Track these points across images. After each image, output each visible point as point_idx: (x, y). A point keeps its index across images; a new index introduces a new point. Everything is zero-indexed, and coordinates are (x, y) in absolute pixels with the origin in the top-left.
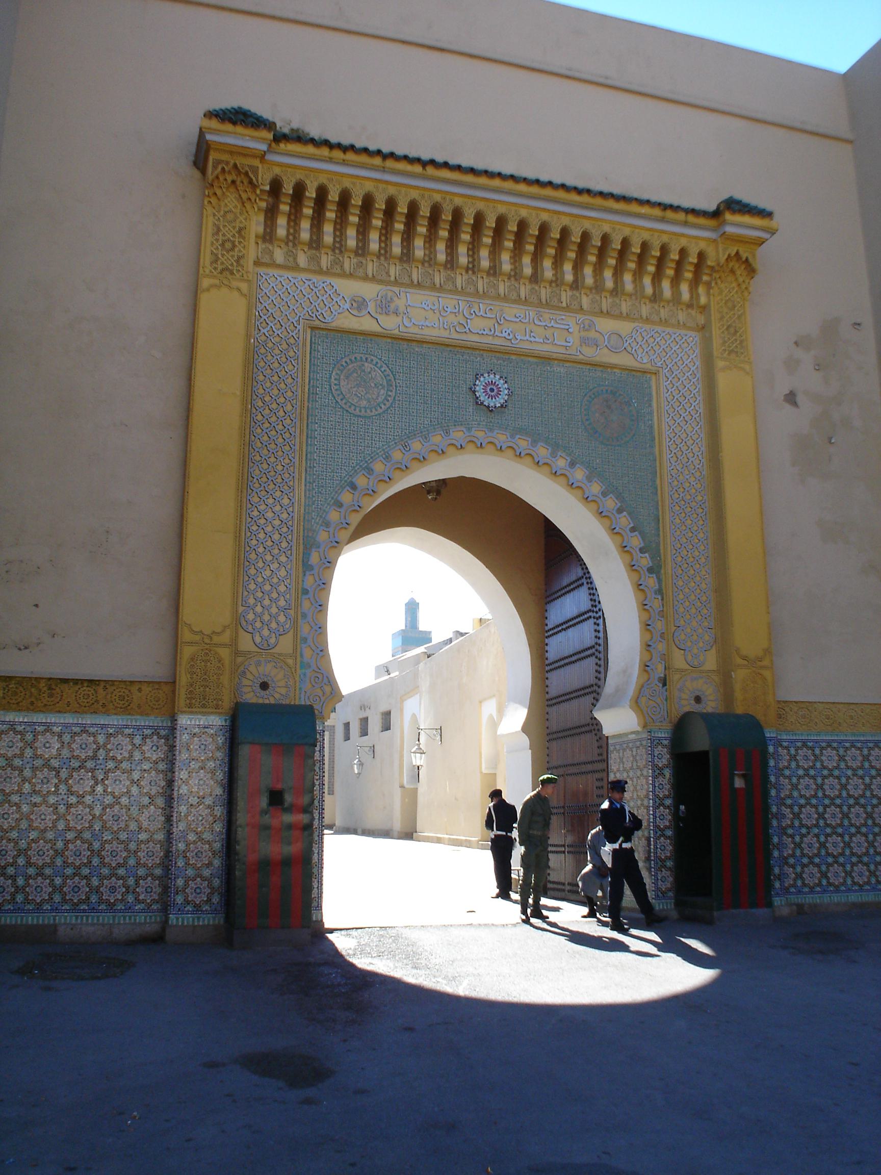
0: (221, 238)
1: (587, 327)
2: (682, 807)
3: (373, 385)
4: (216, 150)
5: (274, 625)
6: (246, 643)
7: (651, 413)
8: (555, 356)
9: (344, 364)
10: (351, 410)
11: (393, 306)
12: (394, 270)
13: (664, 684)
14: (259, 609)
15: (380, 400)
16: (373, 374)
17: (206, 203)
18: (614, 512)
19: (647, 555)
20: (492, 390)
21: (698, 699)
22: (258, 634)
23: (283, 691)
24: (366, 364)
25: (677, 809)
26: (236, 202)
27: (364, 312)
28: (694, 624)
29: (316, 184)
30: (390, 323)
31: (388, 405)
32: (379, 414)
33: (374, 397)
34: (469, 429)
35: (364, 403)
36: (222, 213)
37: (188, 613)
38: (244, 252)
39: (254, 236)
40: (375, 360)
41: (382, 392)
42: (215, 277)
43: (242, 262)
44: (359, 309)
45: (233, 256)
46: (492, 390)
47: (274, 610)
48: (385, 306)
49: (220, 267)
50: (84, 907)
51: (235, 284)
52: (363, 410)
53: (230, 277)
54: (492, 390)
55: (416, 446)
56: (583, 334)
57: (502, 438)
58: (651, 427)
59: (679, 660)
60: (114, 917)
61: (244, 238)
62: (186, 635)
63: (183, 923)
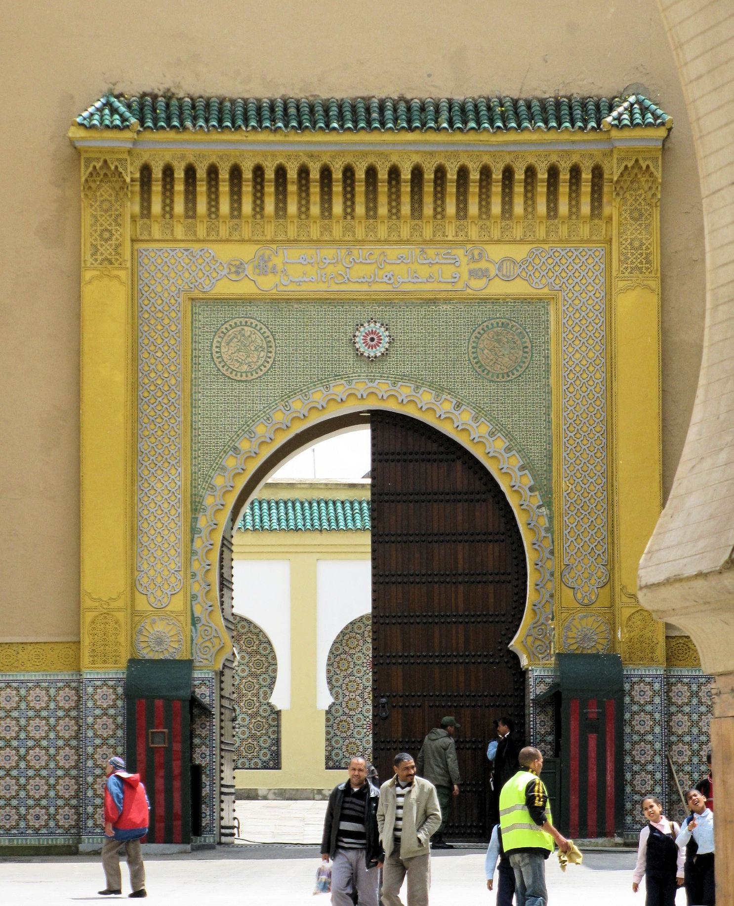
0: (99, 228)
1: (476, 257)
3: (253, 348)
4: (86, 152)
6: (142, 604)
9: (225, 331)
10: (233, 376)
11: (270, 265)
12: (270, 230)
15: (260, 362)
17: (82, 196)
18: (503, 452)
19: (537, 493)
20: (373, 339)
22: (152, 596)
24: (246, 328)
26: (110, 191)
27: (242, 275)
29: (183, 165)
30: (268, 284)
31: (268, 366)
32: (260, 377)
34: (350, 382)
35: (245, 368)
36: (98, 203)
37: (88, 584)
38: (116, 265)
39: (129, 216)
40: (255, 322)
41: (262, 354)
42: (95, 269)
43: (119, 250)
44: (237, 273)
45: (111, 245)
46: (373, 339)
48: (263, 267)
49: (100, 258)
50: (14, 831)
51: (116, 272)
52: (244, 375)
53: (109, 266)
54: (372, 340)
56: (474, 266)
57: (384, 387)
60: (39, 839)
61: (120, 225)
62: (87, 602)
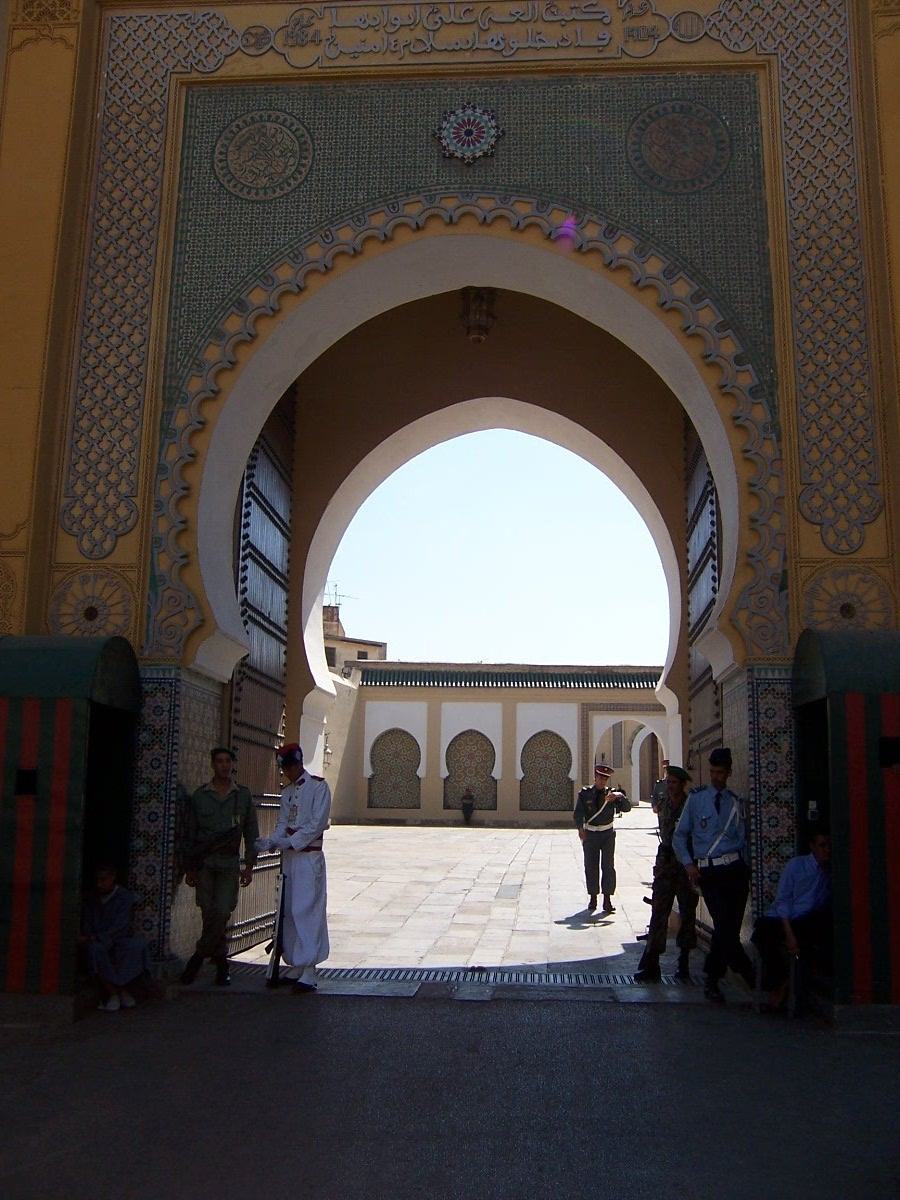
2: (813, 805)
3: (278, 153)
5: (110, 522)
7: (758, 134)
8: (577, 65)
10: (244, 195)
13: (783, 587)
14: (89, 500)
15: (288, 172)
16: (279, 136)
20: (469, 133)
21: (847, 610)
23: (119, 620)
24: (268, 124)
25: (803, 807)
28: (840, 478)
30: (304, 58)
33: (280, 170)
44: (258, 45)
46: (469, 133)
47: (111, 500)
49: (36, 11)
51: (57, 33)
52: (261, 192)
55: (345, 235)
58: (757, 156)
59: (810, 544)
63: (518, 980)
